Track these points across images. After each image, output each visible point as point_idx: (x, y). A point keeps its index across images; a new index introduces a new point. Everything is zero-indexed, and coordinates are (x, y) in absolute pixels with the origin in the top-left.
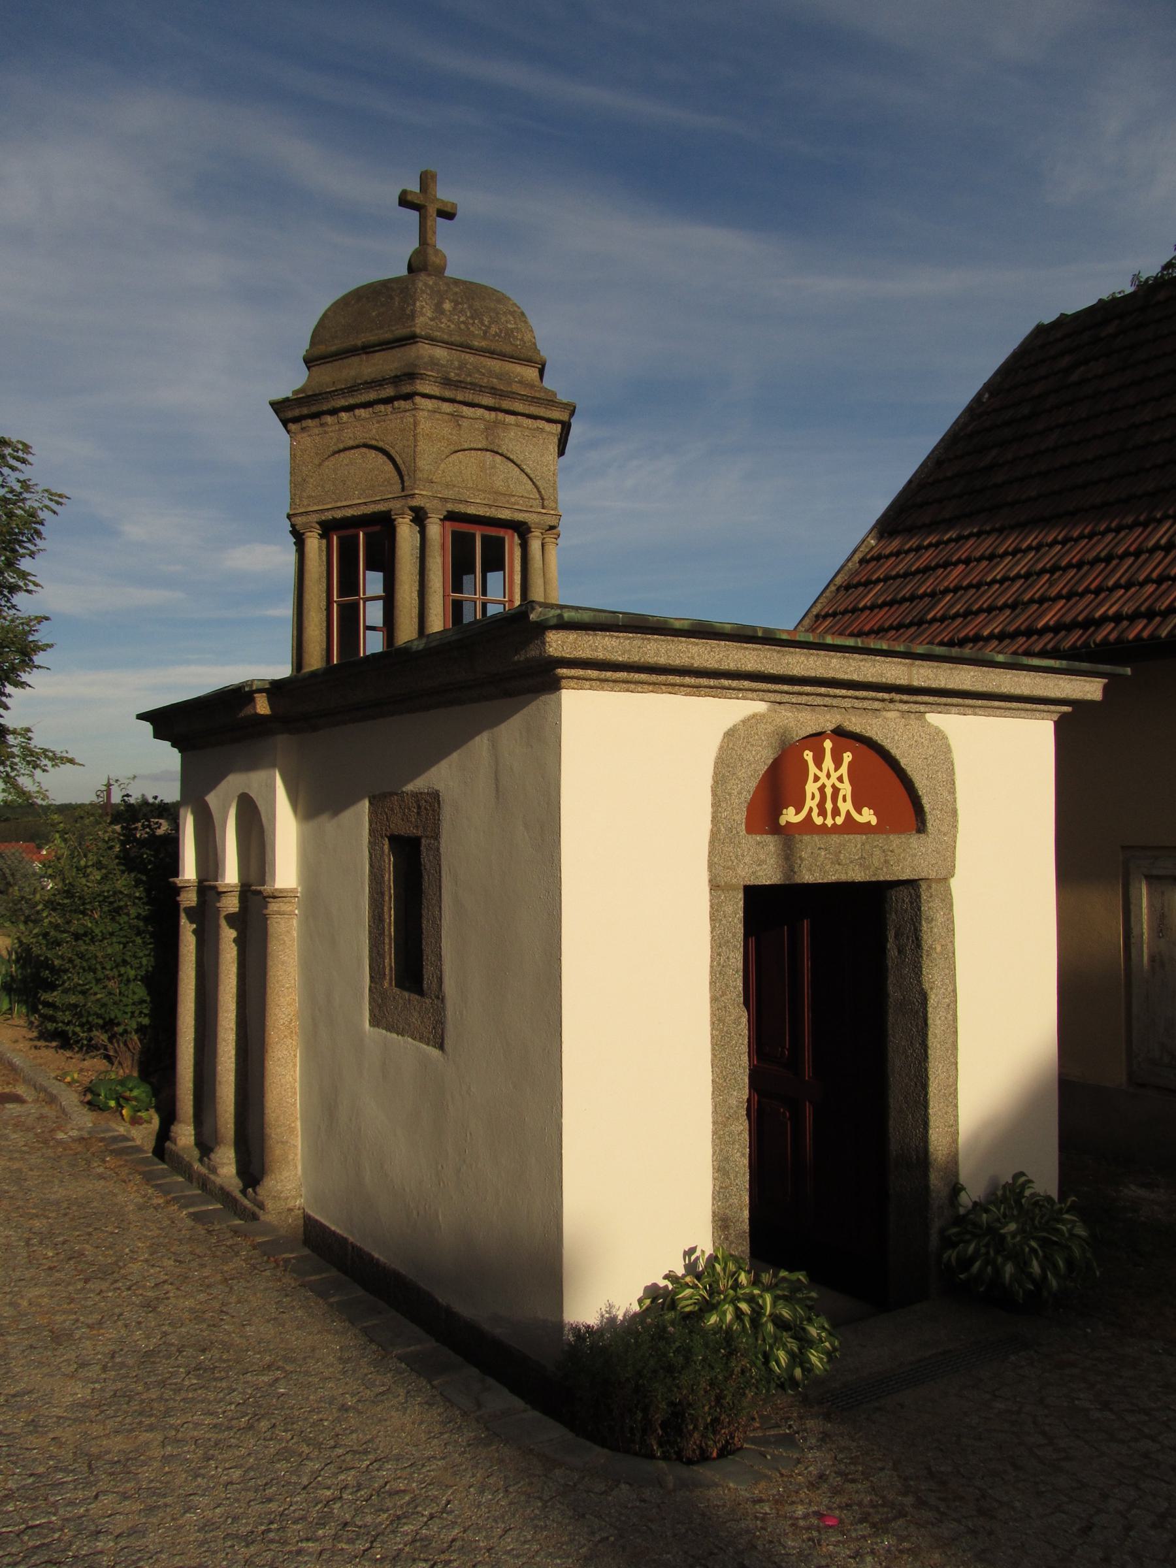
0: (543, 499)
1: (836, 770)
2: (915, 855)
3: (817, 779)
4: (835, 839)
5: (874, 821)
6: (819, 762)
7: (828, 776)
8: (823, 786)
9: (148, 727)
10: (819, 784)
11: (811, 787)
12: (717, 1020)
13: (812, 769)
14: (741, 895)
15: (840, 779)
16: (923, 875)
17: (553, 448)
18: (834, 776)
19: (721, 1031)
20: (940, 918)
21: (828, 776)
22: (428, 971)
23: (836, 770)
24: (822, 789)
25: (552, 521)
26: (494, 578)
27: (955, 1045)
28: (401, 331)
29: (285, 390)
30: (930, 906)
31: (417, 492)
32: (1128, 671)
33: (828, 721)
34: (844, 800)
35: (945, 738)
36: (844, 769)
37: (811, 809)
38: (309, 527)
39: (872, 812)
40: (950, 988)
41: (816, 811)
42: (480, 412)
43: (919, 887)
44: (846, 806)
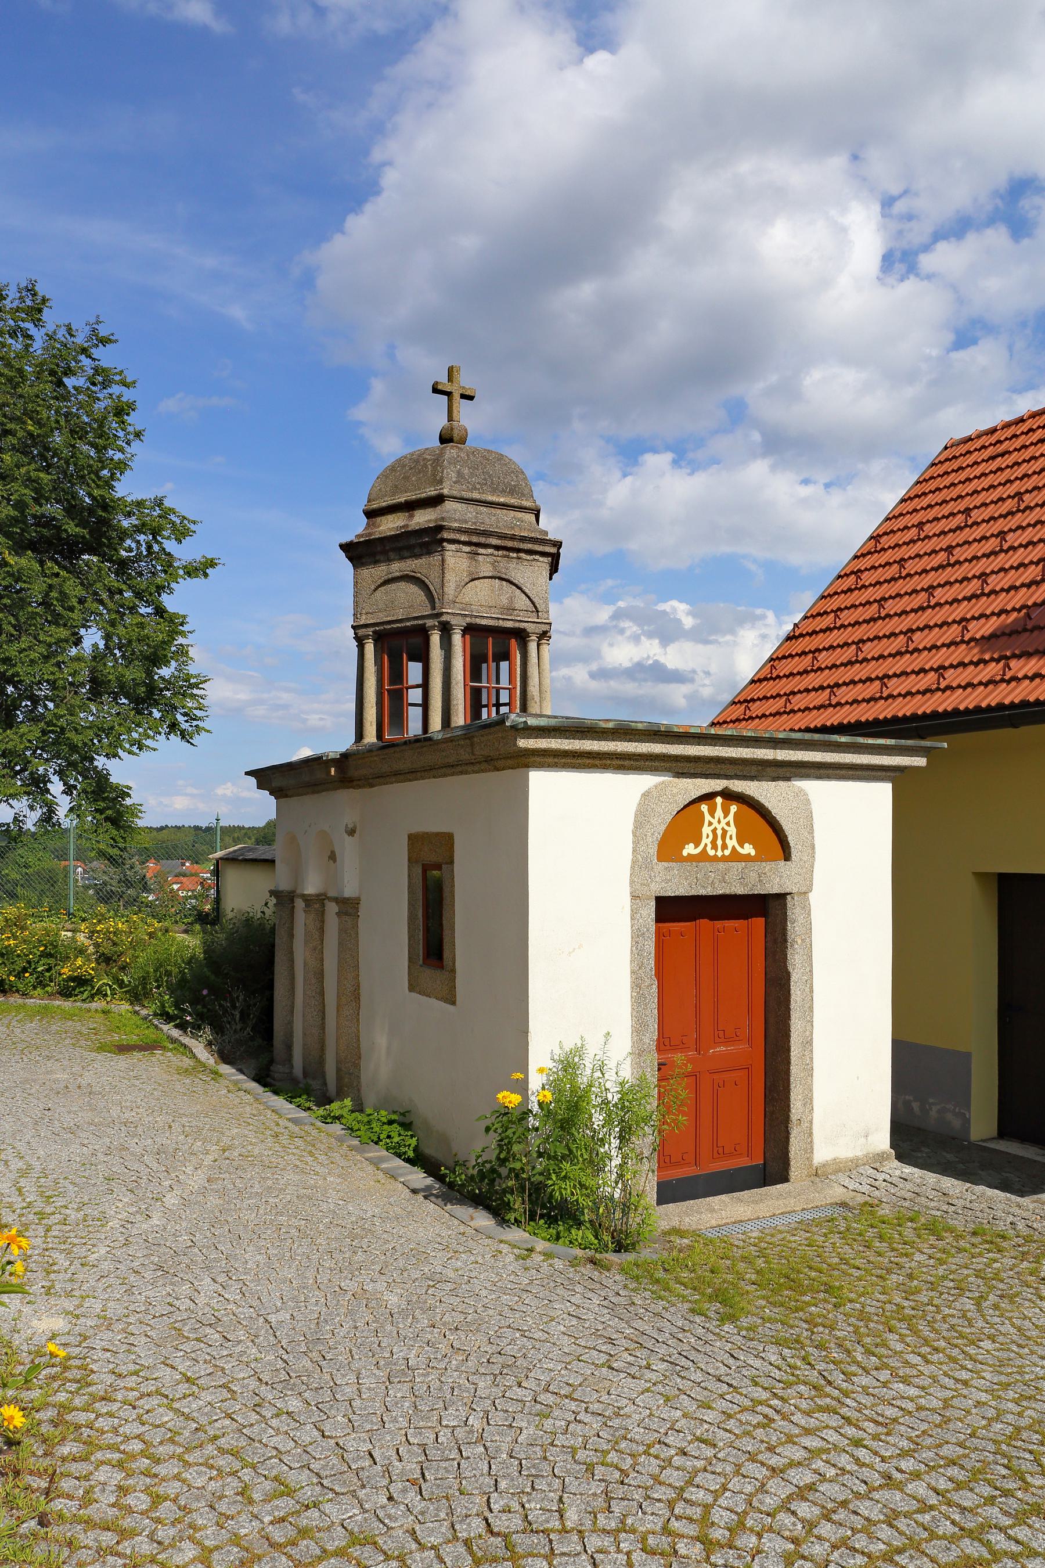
0: (538, 611)
1: (725, 817)
2: (781, 877)
3: (710, 824)
4: (721, 865)
5: (753, 853)
6: (712, 813)
7: (719, 822)
8: (716, 829)
9: (252, 781)
10: (712, 827)
11: (706, 830)
12: (637, 985)
13: (708, 817)
14: (653, 903)
15: (728, 824)
16: (788, 891)
17: (546, 574)
18: (724, 822)
19: (638, 993)
20: (801, 919)
21: (719, 822)
22: (446, 955)
23: (725, 817)
24: (714, 831)
25: (545, 628)
26: (504, 665)
27: (811, 1008)
28: (431, 492)
29: (349, 537)
30: (794, 911)
31: (444, 610)
32: (945, 745)
33: (717, 785)
34: (731, 838)
35: (806, 794)
36: (731, 818)
37: (706, 845)
38: (367, 637)
39: (751, 846)
40: (808, 969)
41: (709, 846)
42: (490, 551)
43: (786, 899)
44: (732, 843)
